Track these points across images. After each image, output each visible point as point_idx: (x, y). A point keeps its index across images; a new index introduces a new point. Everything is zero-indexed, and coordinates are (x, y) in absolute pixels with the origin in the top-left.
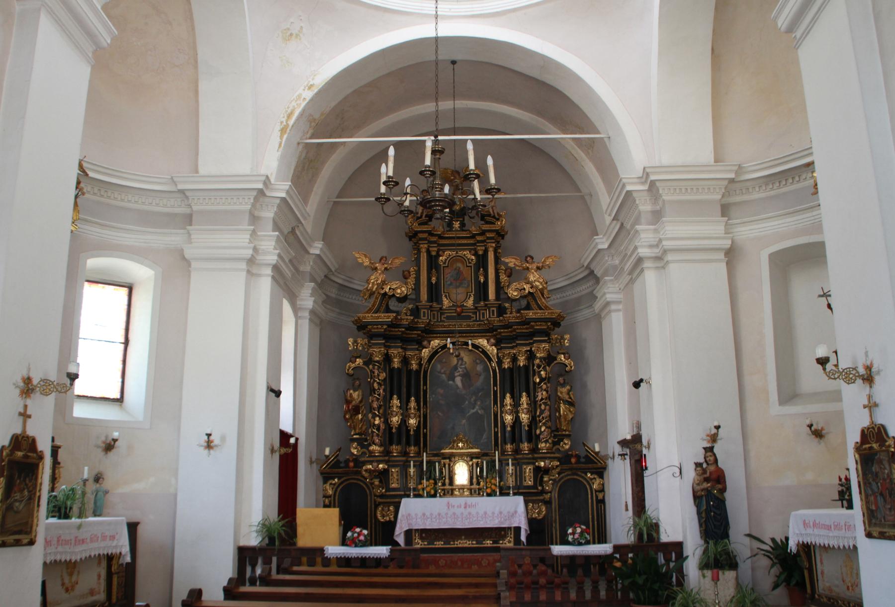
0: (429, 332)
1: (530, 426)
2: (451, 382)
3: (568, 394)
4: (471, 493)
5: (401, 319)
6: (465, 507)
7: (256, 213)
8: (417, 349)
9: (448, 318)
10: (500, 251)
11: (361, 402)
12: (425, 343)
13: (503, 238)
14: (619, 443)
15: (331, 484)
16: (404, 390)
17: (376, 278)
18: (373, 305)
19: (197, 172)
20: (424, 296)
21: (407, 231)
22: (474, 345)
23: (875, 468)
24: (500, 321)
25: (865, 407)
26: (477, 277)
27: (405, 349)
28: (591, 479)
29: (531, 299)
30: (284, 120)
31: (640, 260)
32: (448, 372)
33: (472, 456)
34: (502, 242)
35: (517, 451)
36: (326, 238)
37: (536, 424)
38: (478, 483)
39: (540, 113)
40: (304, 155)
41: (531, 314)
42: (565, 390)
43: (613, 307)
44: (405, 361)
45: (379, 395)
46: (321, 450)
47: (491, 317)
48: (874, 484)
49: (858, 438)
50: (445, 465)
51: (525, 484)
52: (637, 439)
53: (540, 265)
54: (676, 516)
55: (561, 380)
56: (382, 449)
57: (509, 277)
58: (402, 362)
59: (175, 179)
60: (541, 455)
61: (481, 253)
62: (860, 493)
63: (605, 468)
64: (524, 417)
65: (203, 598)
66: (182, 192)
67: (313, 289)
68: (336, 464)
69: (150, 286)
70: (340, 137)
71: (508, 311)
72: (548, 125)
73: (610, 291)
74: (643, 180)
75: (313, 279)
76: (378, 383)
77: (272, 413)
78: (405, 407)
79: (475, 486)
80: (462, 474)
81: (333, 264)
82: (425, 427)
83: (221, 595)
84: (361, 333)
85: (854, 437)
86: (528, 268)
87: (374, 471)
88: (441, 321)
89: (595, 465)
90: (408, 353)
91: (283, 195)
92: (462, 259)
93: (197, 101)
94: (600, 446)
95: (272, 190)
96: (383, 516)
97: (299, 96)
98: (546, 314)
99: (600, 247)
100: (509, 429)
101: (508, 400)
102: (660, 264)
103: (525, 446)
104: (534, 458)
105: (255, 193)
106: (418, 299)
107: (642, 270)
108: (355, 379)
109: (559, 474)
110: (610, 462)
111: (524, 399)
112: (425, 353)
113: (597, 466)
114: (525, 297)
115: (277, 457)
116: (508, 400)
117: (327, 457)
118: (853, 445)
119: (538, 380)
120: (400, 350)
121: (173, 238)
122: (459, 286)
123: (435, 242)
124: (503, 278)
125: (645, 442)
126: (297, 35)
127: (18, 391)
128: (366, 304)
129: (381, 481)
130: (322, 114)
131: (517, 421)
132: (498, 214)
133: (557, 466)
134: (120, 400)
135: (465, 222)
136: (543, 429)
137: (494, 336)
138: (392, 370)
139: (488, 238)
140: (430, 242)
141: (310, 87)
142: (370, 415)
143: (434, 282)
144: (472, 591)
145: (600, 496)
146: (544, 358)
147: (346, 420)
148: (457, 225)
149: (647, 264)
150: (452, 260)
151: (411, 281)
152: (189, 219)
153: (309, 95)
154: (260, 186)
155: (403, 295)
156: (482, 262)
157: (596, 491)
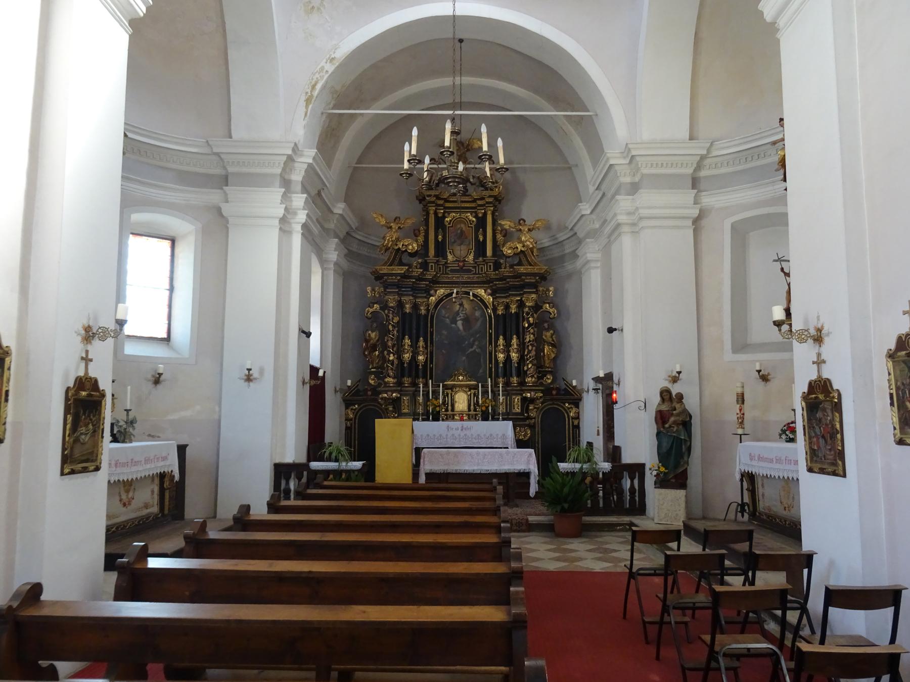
0: (436, 282)
7: (286, 177)
8: (425, 297)
9: (452, 271)
18: (389, 259)
19: (231, 137)
20: (432, 252)
22: (474, 295)
23: (819, 415)
24: (496, 275)
25: (814, 363)
27: (416, 297)
29: (522, 256)
30: (309, 91)
31: (618, 225)
33: (470, 388)
36: (348, 199)
38: (475, 410)
39: (536, 91)
41: (522, 269)
42: (548, 334)
43: (593, 265)
44: (415, 307)
46: (343, 381)
48: (817, 428)
49: (806, 389)
51: (514, 411)
52: (609, 377)
54: (639, 443)
55: (546, 325)
56: (395, 380)
59: (210, 143)
61: (480, 215)
62: (805, 435)
63: (580, 399)
64: (514, 356)
65: (251, 512)
66: (218, 154)
68: (357, 393)
69: (191, 239)
70: (358, 108)
71: (503, 266)
72: (543, 103)
73: (591, 252)
74: (625, 154)
75: (337, 236)
77: (304, 350)
78: (414, 345)
79: (472, 412)
80: (461, 401)
81: (354, 222)
82: (431, 362)
83: (265, 509)
85: (801, 387)
88: (447, 274)
89: (572, 397)
91: (311, 161)
93: (227, 69)
95: (302, 155)
97: (322, 68)
98: (535, 270)
99: (583, 213)
101: (501, 341)
103: (515, 380)
105: (285, 158)
106: (427, 254)
107: (620, 235)
109: (542, 403)
110: (585, 395)
111: (514, 341)
113: (575, 398)
114: (518, 254)
115: (307, 387)
116: (501, 341)
118: (801, 395)
121: (213, 196)
123: (441, 205)
124: (499, 237)
125: (615, 379)
126: (319, 9)
127: (80, 338)
128: (382, 257)
129: (394, 408)
131: (508, 359)
134: (168, 340)
137: (491, 288)
138: (404, 314)
139: (488, 203)
142: (386, 352)
145: (576, 422)
149: (626, 229)
150: (455, 221)
151: (421, 239)
152: (224, 180)
153: (330, 68)
154: (290, 152)
156: (481, 223)
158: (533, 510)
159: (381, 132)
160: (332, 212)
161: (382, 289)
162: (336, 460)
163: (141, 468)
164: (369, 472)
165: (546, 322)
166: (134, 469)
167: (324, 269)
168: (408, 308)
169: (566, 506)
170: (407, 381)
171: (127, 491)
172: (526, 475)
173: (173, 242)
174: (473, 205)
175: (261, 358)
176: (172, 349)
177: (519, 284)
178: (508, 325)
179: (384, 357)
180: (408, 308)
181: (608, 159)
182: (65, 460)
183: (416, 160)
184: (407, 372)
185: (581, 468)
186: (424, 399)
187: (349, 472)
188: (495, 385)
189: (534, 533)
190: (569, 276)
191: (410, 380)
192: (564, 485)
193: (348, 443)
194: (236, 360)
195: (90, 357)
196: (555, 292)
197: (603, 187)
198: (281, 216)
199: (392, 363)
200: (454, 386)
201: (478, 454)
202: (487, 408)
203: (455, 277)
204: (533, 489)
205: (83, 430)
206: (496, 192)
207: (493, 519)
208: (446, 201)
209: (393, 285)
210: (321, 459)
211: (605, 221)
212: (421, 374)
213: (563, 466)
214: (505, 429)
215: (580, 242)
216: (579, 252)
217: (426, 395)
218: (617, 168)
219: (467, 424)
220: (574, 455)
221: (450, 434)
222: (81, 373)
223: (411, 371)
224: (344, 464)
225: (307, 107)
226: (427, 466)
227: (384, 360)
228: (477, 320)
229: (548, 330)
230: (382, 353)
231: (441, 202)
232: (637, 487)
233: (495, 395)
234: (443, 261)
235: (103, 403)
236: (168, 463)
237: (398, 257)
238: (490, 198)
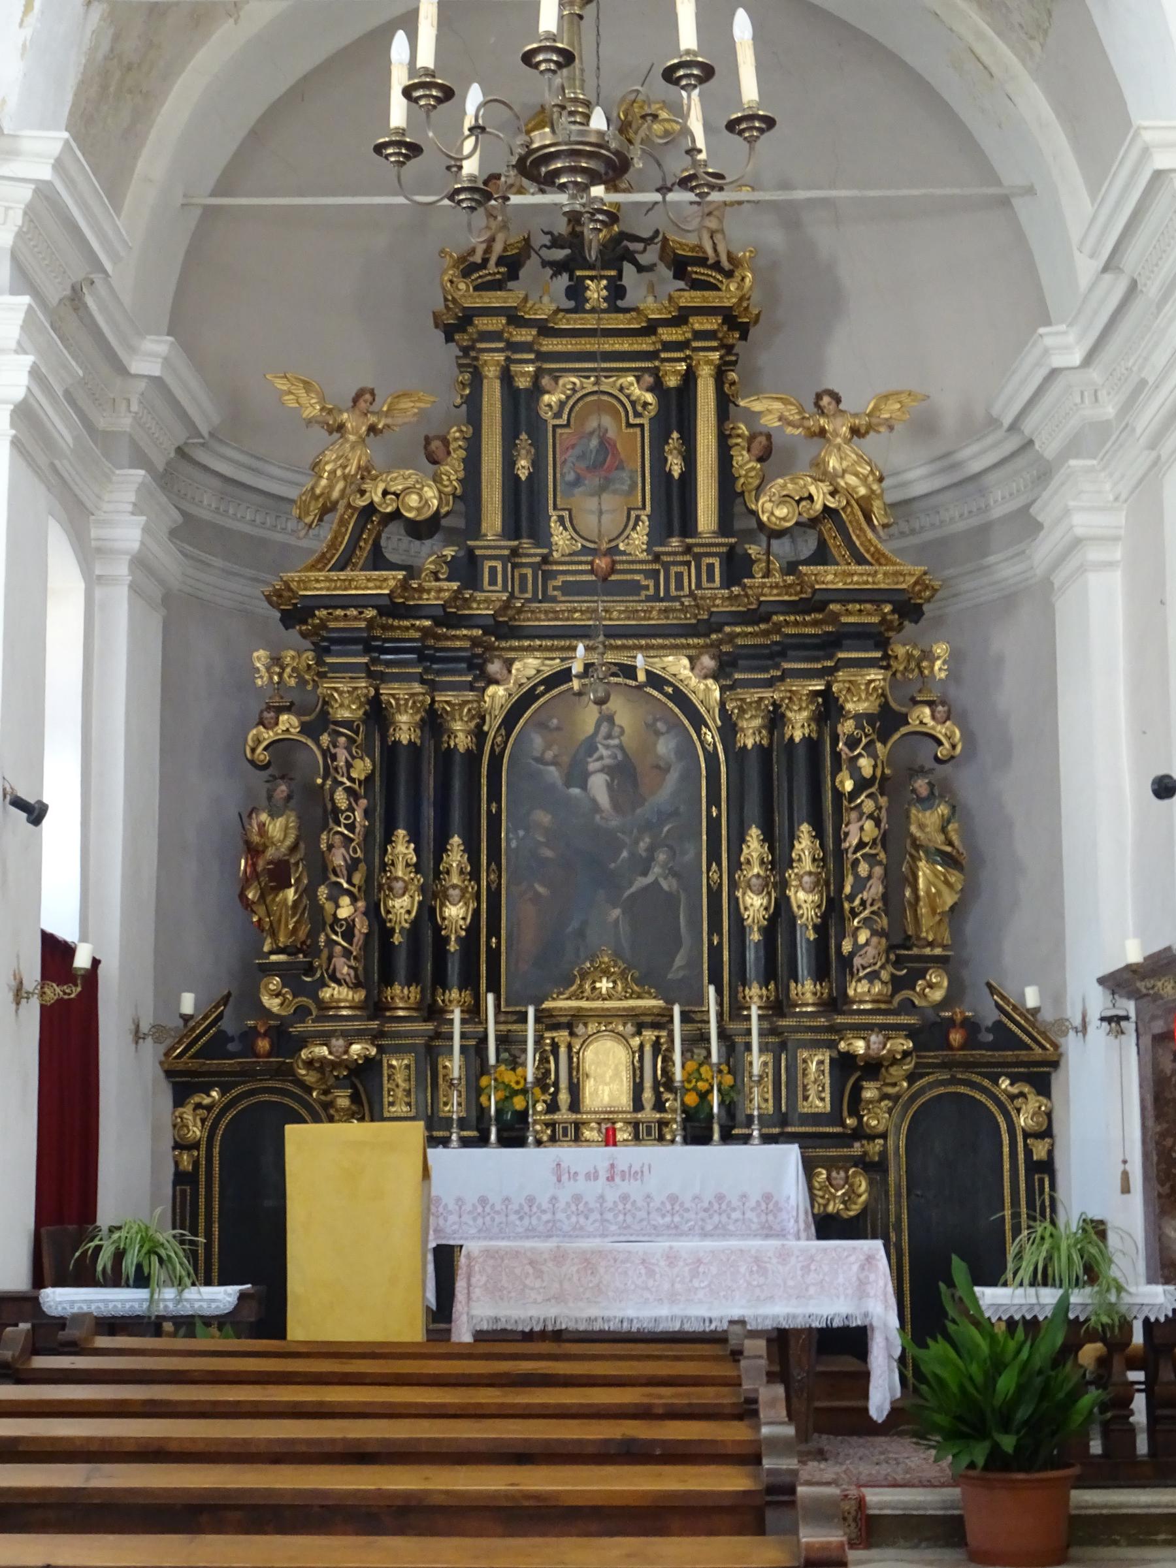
0: (505, 630)
1: (821, 929)
2: (576, 791)
3: (943, 830)
4: (637, 1138)
5: (421, 590)
6: (611, 1179)
9: (567, 589)
10: (733, 376)
11: (294, 848)
12: (494, 668)
13: (744, 337)
14: (1102, 981)
15: (198, 1106)
16: (429, 813)
17: (340, 460)
18: (333, 545)
20: (493, 519)
21: (440, 306)
24: (732, 598)
27: (433, 687)
28: (1013, 1097)
29: (827, 530)
32: (565, 759)
34: (740, 347)
36: (178, 325)
37: (842, 920)
38: (659, 1106)
40: (105, 47)
43: (1094, 554)
44: (433, 722)
45: (351, 827)
46: (166, 996)
50: (555, 1046)
51: (804, 1108)
53: (862, 422)
56: (360, 995)
57: (760, 460)
58: (422, 725)
60: (856, 1020)
61: (672, 382)
64: (805, 902)
67: (142, 489)
68: (217, 1046)
75: (140, 459)
76: (349, 791)
78: (430, 866)
79: (649, 1114)
80: (607, 1073)
81: (204, 411)
82: (494, 930)
84: (294, 634)
86: (822, 432)
87: (334, 1065)
88: (546, 598)
91: (45, 173)
92: (602, 402)
94: (1042, 994)
98: (879, 578)
99: (1058, 361)
100: (756, 936)
101: (754, 846)
103: (806, 991)
104: (832, 1029)
106: (473, 527)
109: (911, 1078)
110: (1071, 1045)
111: (805, 844)
112: (497, 694)
114: (814, 522)
115: (32, 1013)
117: (186, 1018)
119: (849, 785)
120: (417, 688)
122: (602, 489)
124: (744, 462)
129: (355, 1098)
131: (781, 914)
132: (731, 258)
133: (906, 1054)
135: (625, 282)
136: (863, 937)
138: (391, 751)
139: (699, 335)
140: (513, 347)
143: (523, 475)
144: (667, 1396)
146: (870, 718)
147: (247, 905)
148: (596, 292)
151: (452, 470)
155: (427, 514)
156: (677, 409)
157: (1026, 1135)
158: (885, 1469)
160: (121, 370)
161: (309, 657)
162: (142, 1280)
164: (266, 1313)
165: (922, 771)
167: (92, 581)
168: (405, 727)
169: (1008, 1443)
172: (850, 1340)
174: (645, 344)
177: (825, 634)
178: (781, 785)
179: (317, 910)
180: (405, 727)
183: (434, 92)
184: (401, 962)
185: (1063, 1305)
186: (467, 1065)
187: (187, 1324)
189: (890, 1552)
190: (1009, 601)
192: (997, 1365)
193: (184, 1213)
196: (955, 659)
197: (1131, 259)
202: (704, 1096)
203: (576, 611)
204: (883, 1391)
206: (729, 294)
207: (733, 1433)
208: (545, 329)
209: (346, 641)
210: (84, 1277)
211: (1143, 383)
212: (453, 969)
213: (997, 1300)
214: (774, 1172)
215: (1044, 474)
216: (1044, 513)
217: (475, 1050)
219: (629, 1155)
220: (1033, 1257)
221: (564, 1196)
223: (411, 961)
224: (169, 1293)
226: (475, 1311)
227: (318, 919)
228: (662, 769)
229: (927, 802)
230: (309, 892)
231: (525, 335)
233: (733, 1047)
237: (368, 531)
238: (705, 316)
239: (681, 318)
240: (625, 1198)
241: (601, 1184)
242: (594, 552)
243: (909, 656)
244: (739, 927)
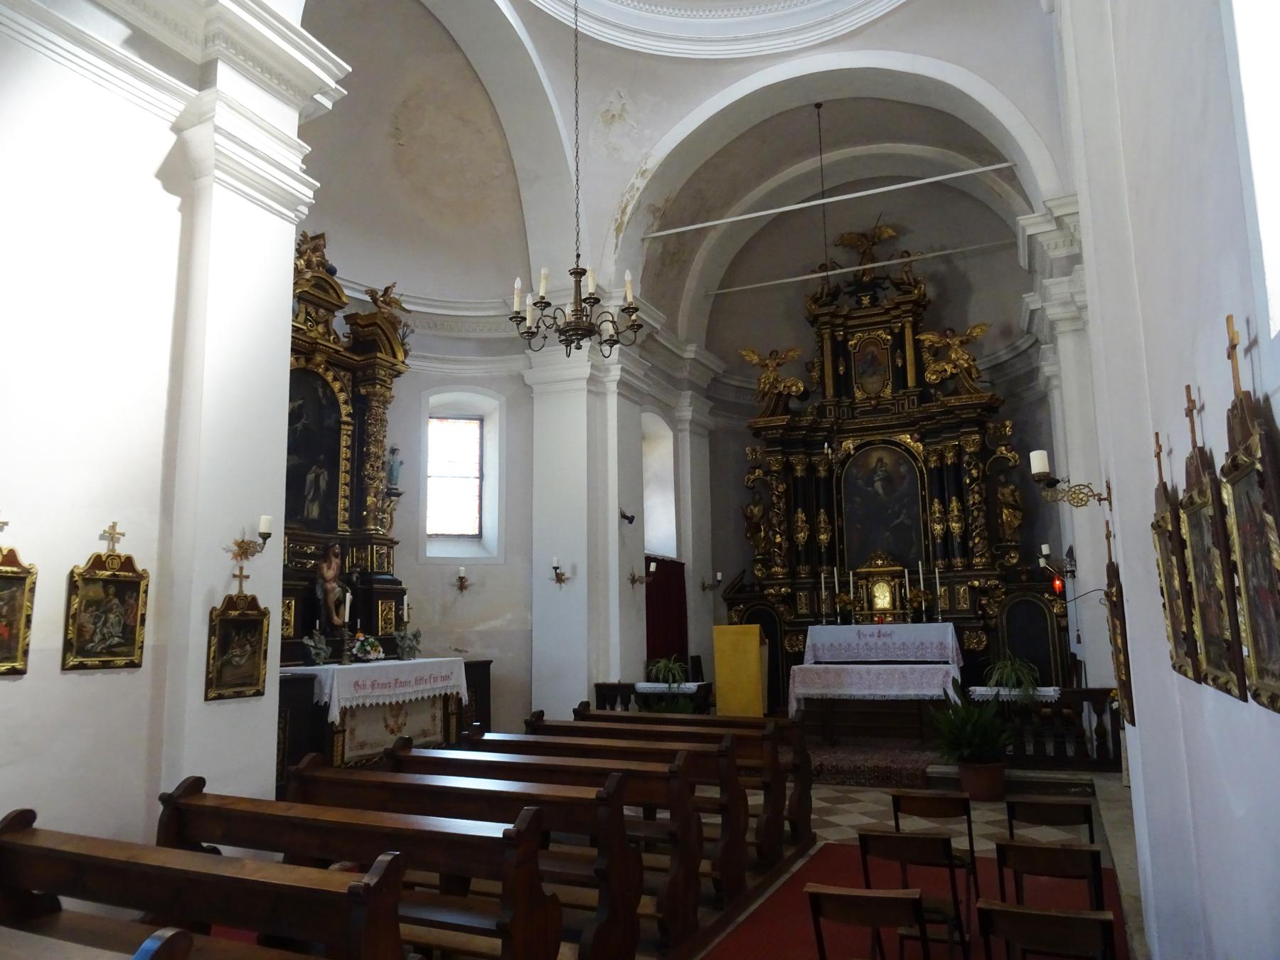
11: (762, 518)
18: (767, 408)
20: (830, 391)
26: (848, 369)
33: (894, 576)
35: (949, 567)
39: (948, 145)
42: (1007, 491)
44: (811, 468)
47: (911, 408)
51: (959, 607)
55: (1002, 478)
69: (496, 415)
75: (693, 386)
79: (899, 611)
80: (883, 598)
81: (715, 364)
82: (841, 542)
90: (814, 459)
92: (877, 342)
96: (792, 646)
97: (633, 186)
102: (1078, 325)
103: (958, 561)
108: (758, 491)
111: (954, 504)
121: (515, 363)
126: (620, 116)
127: (230, 555)
130: (667, 201)
131: (947, 533)
132: (915, 280)
134: (479, 536)
139: (905, 312)
141: (643, 173)
148: (866, 301)
150: (863, 344)
153: (641, 183)
159: (752, 239)
162: (666, 681)
163: (410, 690)
164: (704, 700)
166: (399, 690)
168: (799, 471)
169: (966, 752)
170: (804, 570)
171: (397, 716)
173: (481, 420)
174: (885, 318)
175: (574, 557)
176: (484, 548)
178: (946, 481)
180: (799, 471)
181: (1024, 230)
182: (209, 684)
184: (824, 557)
185: (997, 694)
188: (929, 572)
191: (807, 568)
194: (546, 557)
195: (245, 573)
198: (588, 375)
199: (780, 546)
200: (870, 575)
201: (868, 672)
202: (920, 604)
203: (866, 422)
205: (238, 651)
208: (847, 317)
217: (830, 587)
218: (1040, 238)
221: (862, 643)
222: (234, 591)
225: (617, 237)
227: (769, 541)
229: (1006, 484)
230: (767, 533)
231: (839, 321)
232: (1109, 727)
233: (930, 585)
234: (846, 401)
235: (265, 622)
236: (452, 683)
237: (780, 402)
239: (897, 306)
240: (885, 644)
241: (875, 639)
242: (871, 399)
243: (996, 427)
244: (934, 538)
